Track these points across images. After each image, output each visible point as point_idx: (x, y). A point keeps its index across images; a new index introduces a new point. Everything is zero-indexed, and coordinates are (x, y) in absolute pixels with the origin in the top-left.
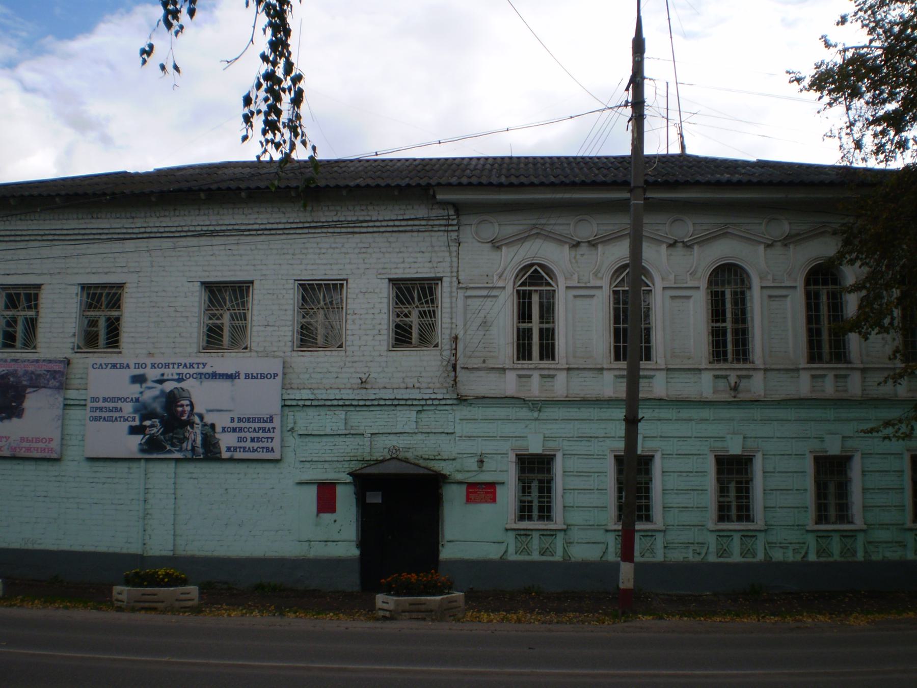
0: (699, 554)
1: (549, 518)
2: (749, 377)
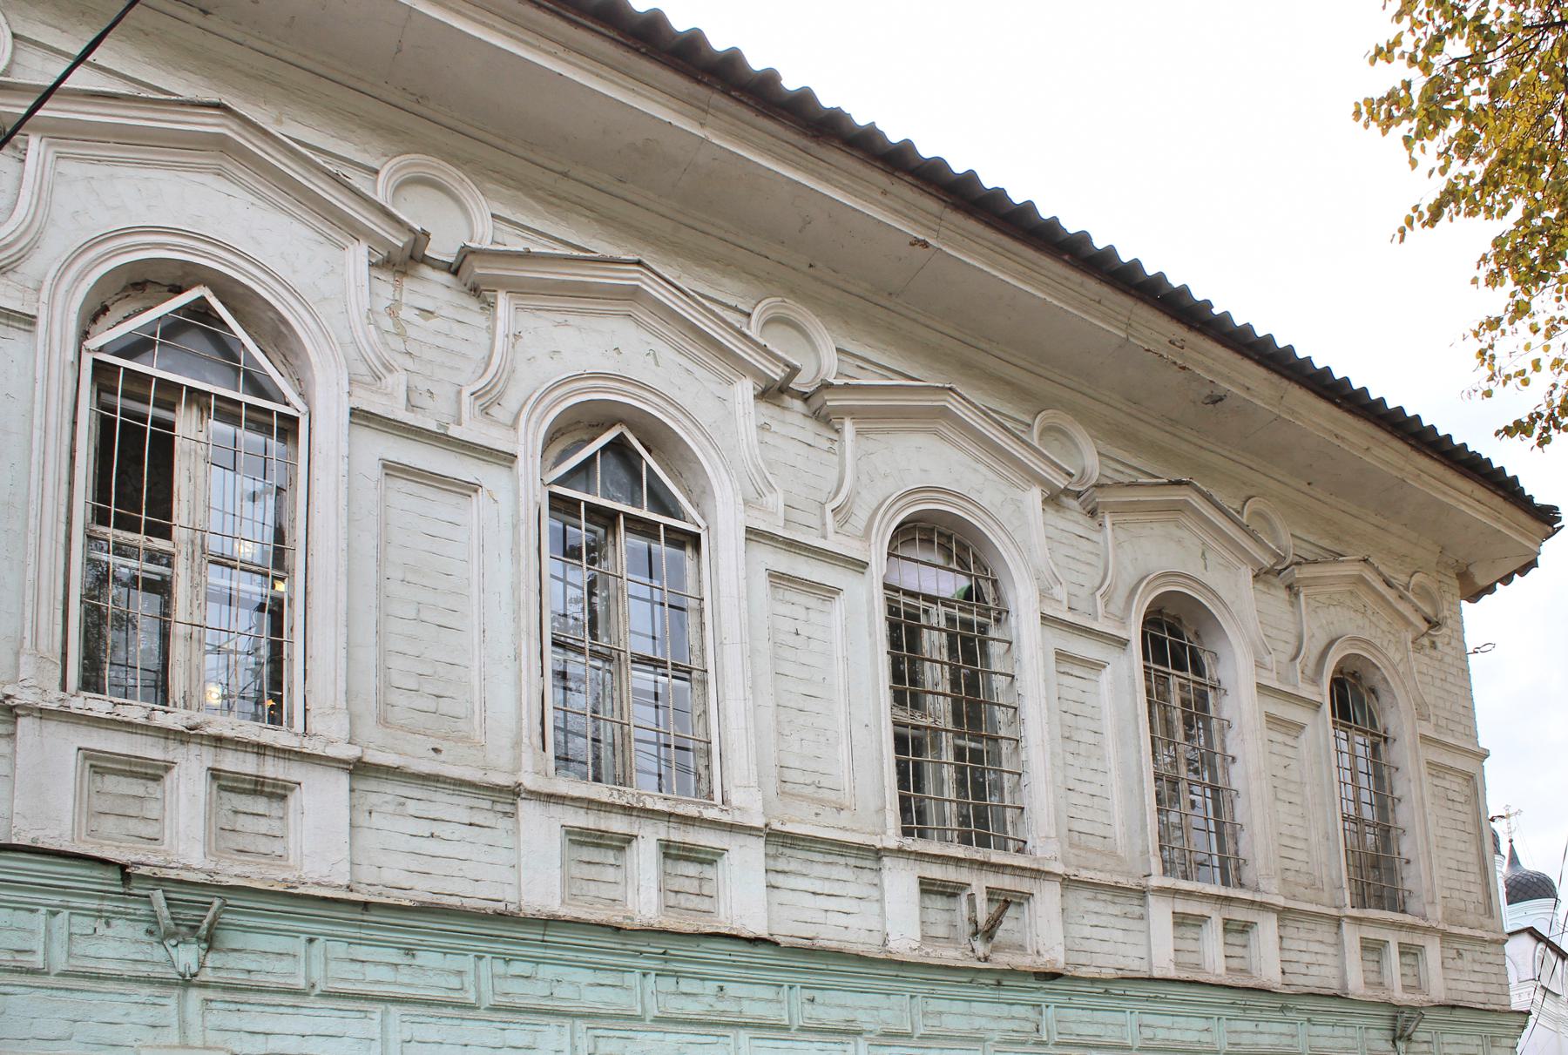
2: (278, 792)
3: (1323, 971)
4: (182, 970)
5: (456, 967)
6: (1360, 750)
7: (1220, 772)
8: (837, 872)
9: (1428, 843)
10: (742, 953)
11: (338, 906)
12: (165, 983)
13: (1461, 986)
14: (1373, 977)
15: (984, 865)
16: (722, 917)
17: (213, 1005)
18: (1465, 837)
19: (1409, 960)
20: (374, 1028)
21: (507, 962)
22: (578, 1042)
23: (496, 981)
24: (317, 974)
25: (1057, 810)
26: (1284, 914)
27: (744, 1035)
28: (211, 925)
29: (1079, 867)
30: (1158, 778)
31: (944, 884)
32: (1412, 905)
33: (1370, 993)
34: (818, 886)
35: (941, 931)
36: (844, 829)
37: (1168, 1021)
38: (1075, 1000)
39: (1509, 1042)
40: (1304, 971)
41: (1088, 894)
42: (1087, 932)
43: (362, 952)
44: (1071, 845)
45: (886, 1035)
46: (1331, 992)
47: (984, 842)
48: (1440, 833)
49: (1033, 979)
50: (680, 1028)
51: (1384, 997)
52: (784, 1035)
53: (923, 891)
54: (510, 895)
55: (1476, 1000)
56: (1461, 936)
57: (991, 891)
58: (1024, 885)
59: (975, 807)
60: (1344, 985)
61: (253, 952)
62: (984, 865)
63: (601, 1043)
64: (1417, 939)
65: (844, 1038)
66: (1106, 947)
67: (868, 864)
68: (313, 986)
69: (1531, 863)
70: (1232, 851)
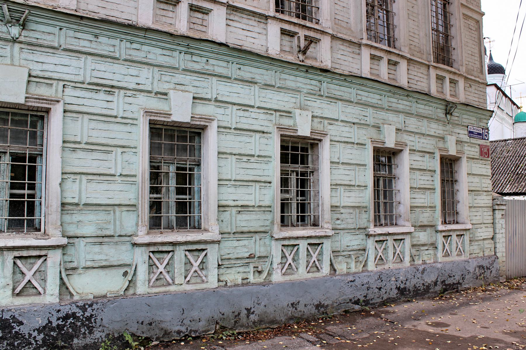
0: (260, 272)
1: (34, 227)
3: (422, 84)
4: (13, 36)
5: (113, 43)
6: (439, 5)
7: (389, 5)
8: (251, 22)
9: (461, 43)
10: (216, 48)
11: (72, 17)
12: (6, 40)
13: (471, 98)
14: (440, 89)
15: (304, 26)
16: (209, 34)
17: (23, 50)
18: (475, 43)
19: (453, 85)
20: (81, 63)
21: (131, 43)
22: (155, 76)
23: (127, 50)
24: (62, 42)
25: (331, 9)
26: (409, 60)
27: (214, 79)
28: (24, 20)
29: (337, 32)
30: (367, 4)
31: (289, 31)
32: (455, 65)
33: (439, 95)
34: (244, 27)
35: (287, 49)
36: (255, 7)
37: (366, 94)
38: (334, 81)
39: (485, 121)
40: (416, 83)
41: (340, 42)
42: (339, 56)
43: (79, 35)
44: (335, 24)
45: (266, 85)
46: (425, 92)
47: (304, 18)
48: (466, 40)
49: (319, 71)
50: (192, 74)
51: (442, 97)
52: (229, 81)
53: (282, 33)
54: (134, 19)
55: (475, 104)
56: (471, 79)
57: (306, 37)
58: (318, 36)
59: (302, 5)
60: (430, 91)
61: (40, 31)
62: (304, 26)
63: (163, 77)
64: (456, 78)
65: (251, 85)
66: (346, 63)
67: (262, 21)
68: (60, 46)
69: (497, 60)
70: (392, 34)
